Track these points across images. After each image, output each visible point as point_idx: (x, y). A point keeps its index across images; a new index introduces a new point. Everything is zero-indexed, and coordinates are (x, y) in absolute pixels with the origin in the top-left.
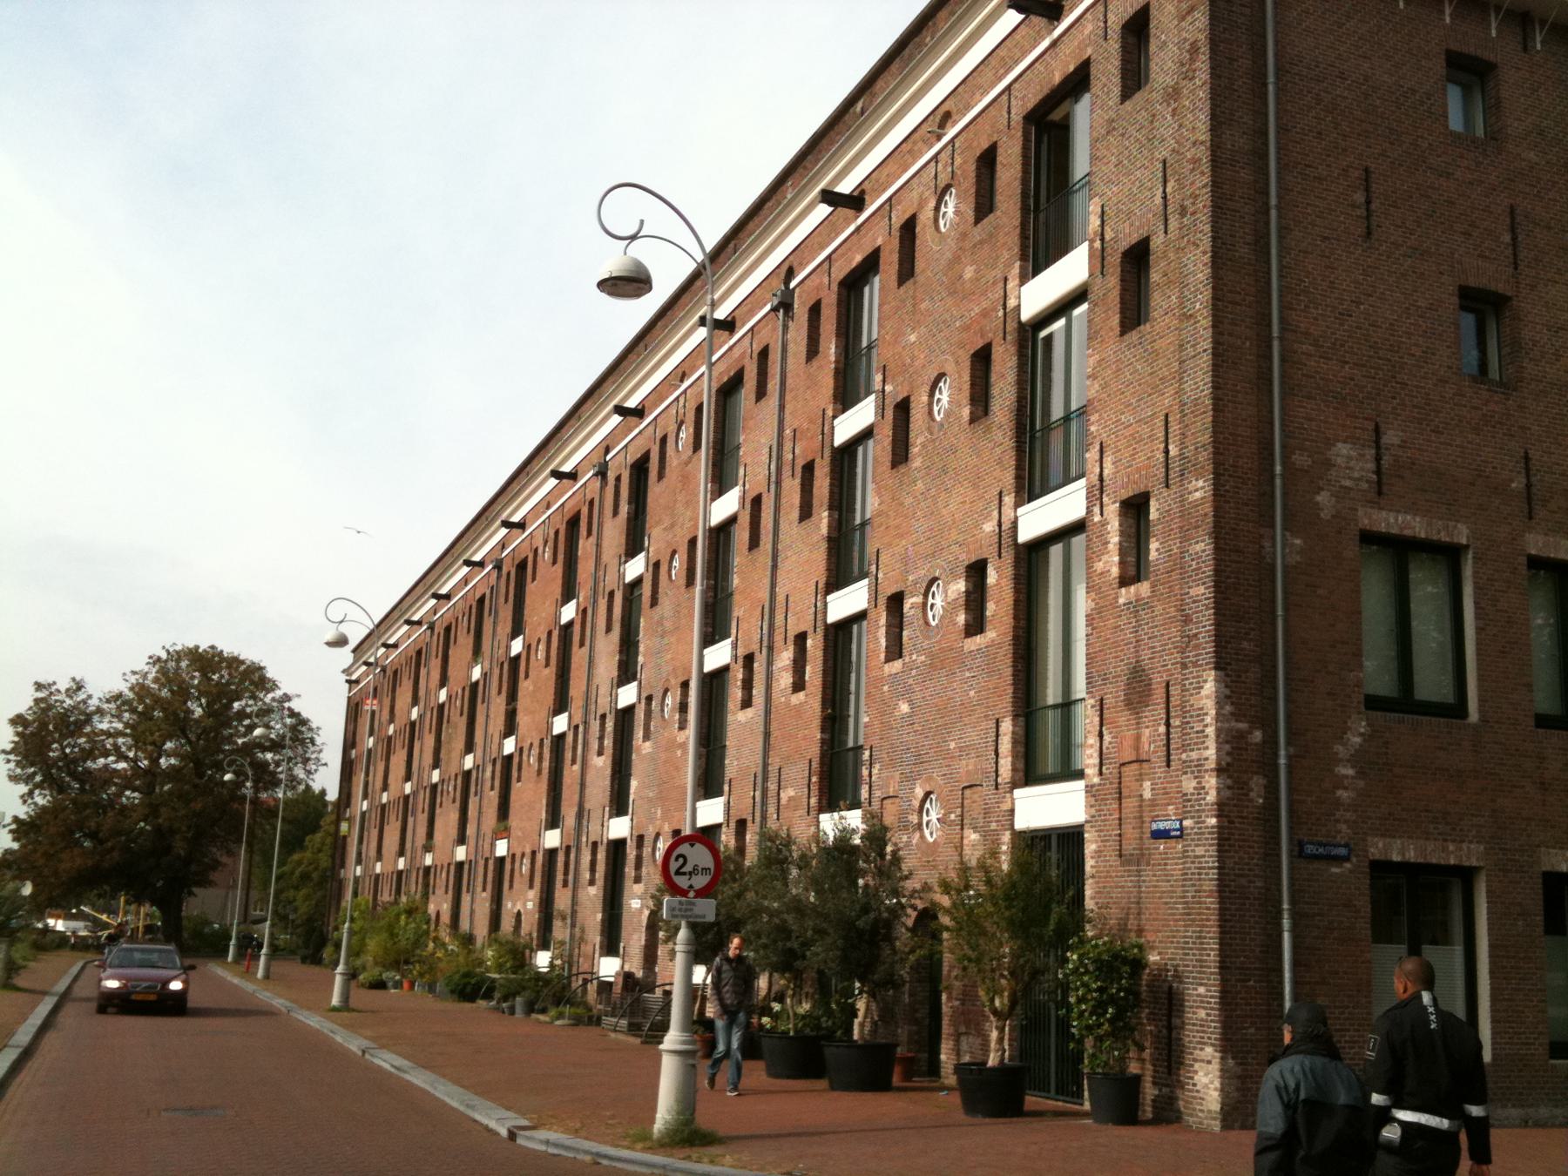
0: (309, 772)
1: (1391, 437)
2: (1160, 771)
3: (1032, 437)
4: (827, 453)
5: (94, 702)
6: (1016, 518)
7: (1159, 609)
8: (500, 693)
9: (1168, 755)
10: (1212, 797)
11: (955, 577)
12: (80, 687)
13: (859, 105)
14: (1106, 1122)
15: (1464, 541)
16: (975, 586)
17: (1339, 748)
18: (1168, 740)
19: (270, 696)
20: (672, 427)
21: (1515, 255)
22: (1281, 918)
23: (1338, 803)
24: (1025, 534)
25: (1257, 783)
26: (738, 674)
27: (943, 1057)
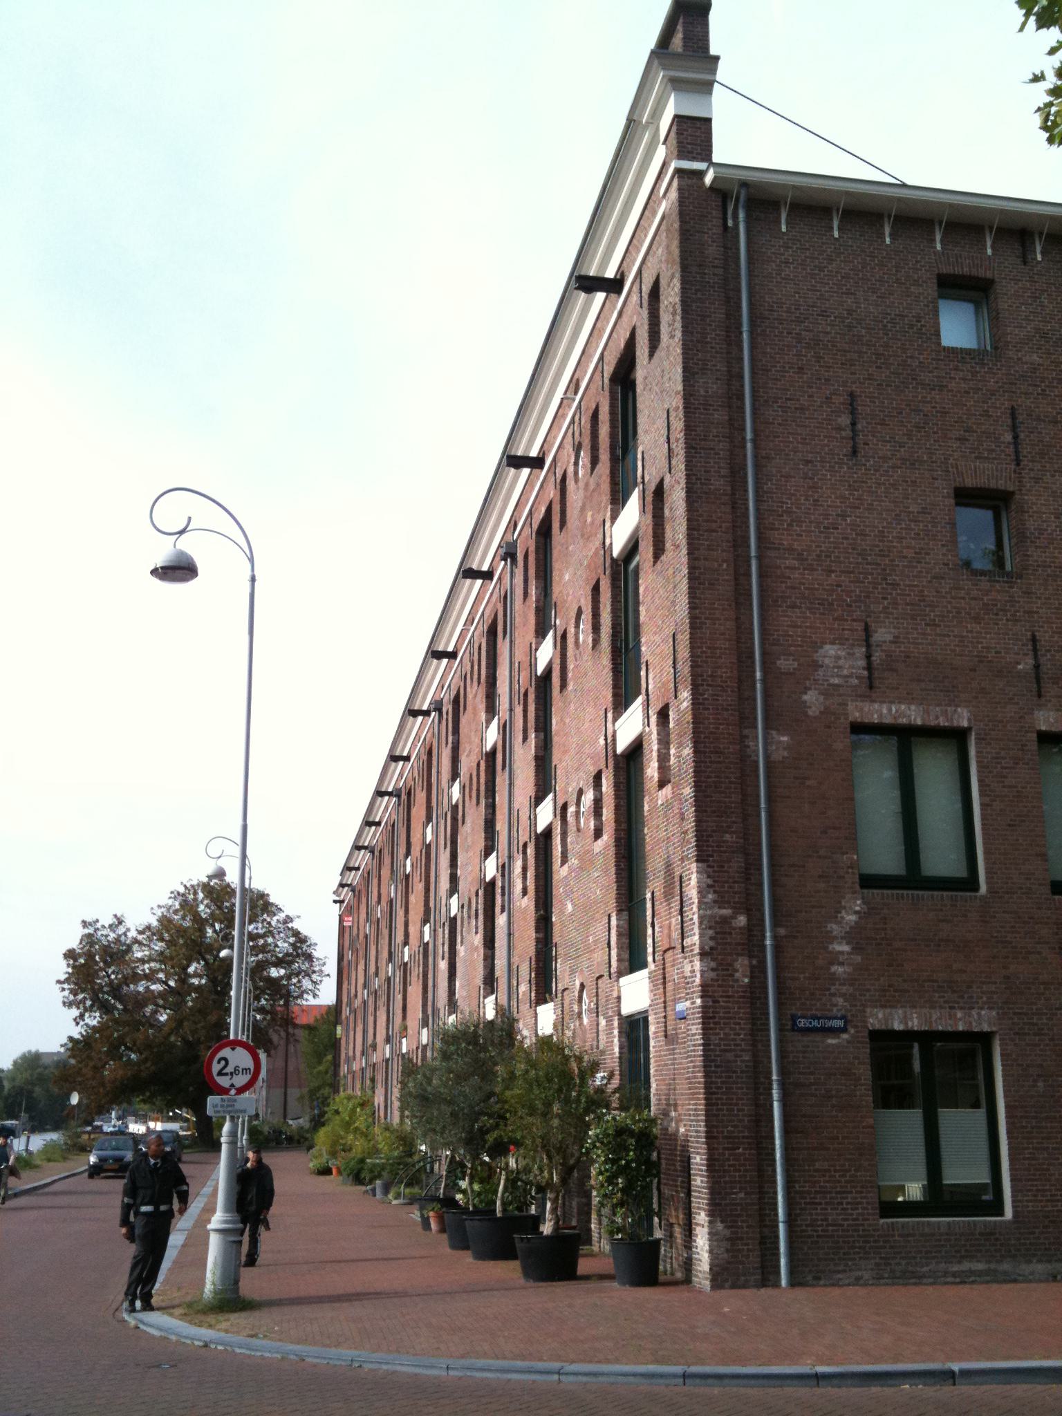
0: (315, 983)
1: (882, 635)
5: (132, 934)
12: (120, 922)
14: (624, 1284)
15: (965, 724)
17: (834, 928)
19: (275, 918)
21: (1017, 452)
22: (771, 1089)
23: (833, 978)
25: (742, 966)
27: (593, 1226)
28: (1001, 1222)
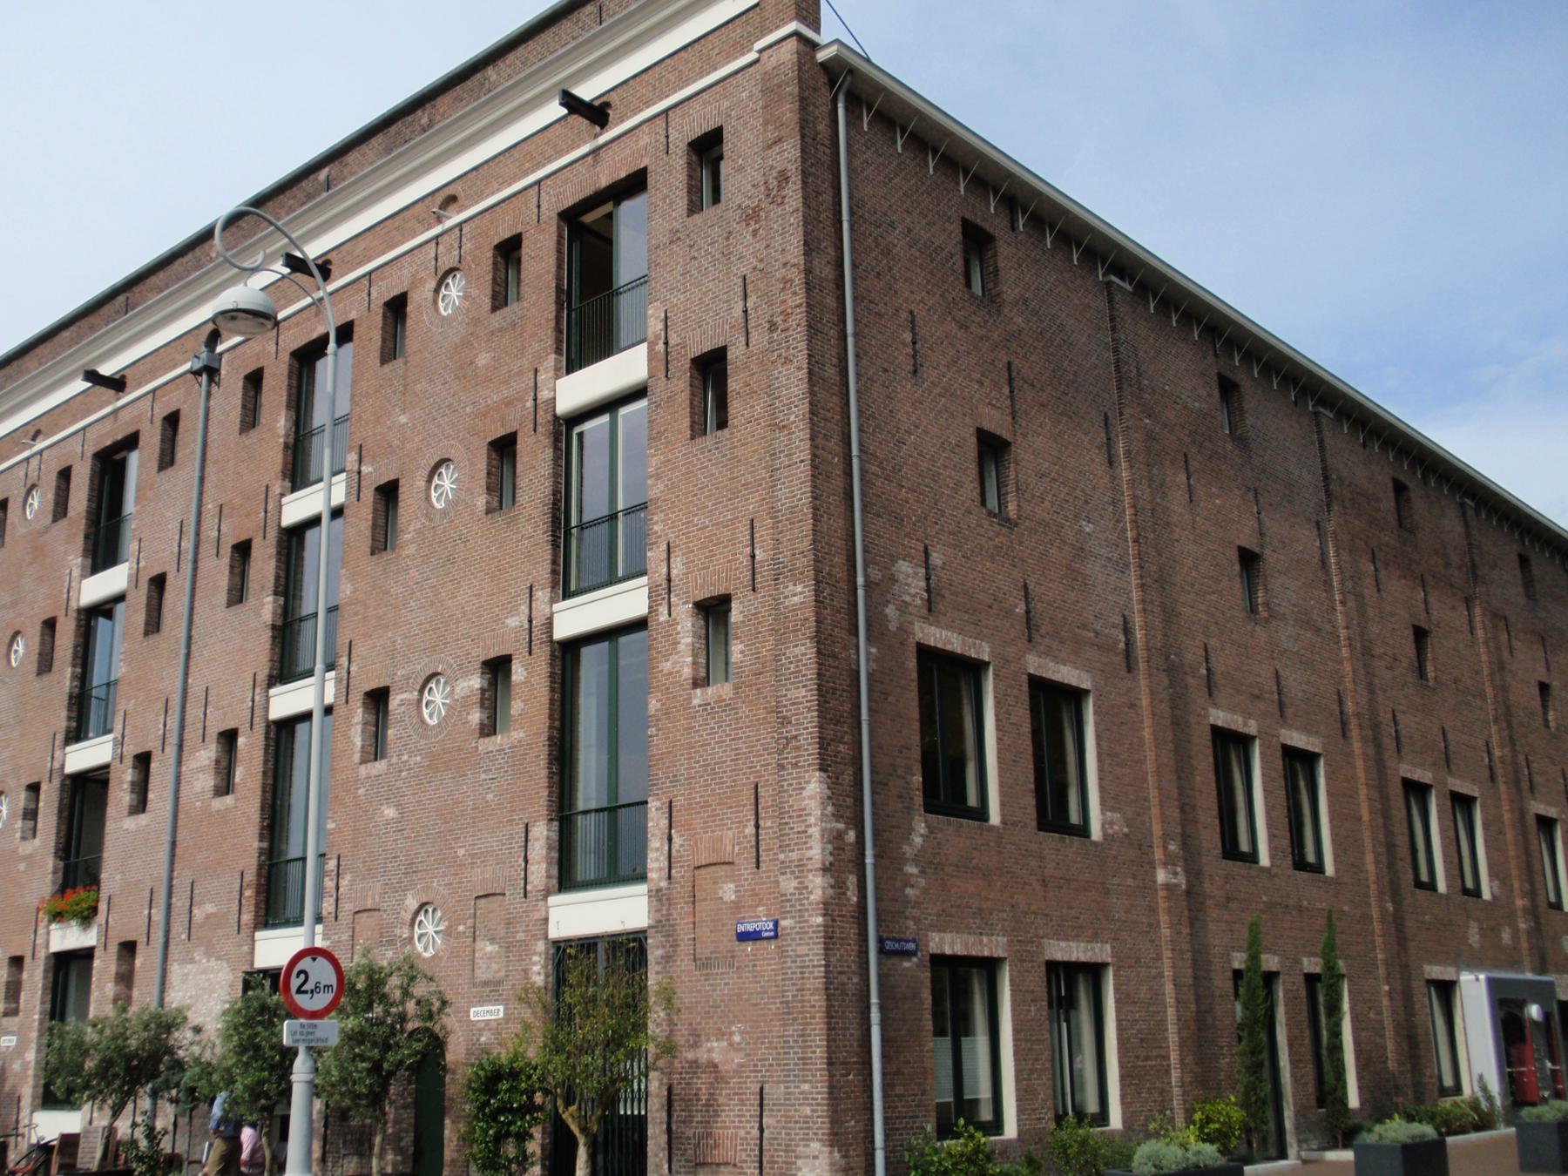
1: (936, 559)
3: (568, 533)
4: (272, 534)
6: (552, 614)
7: (744, 710)
9: (758, 856)
10: (817, 895)
11: (467, 674)
13: (323, 175)
16: (490, 684)
25: (852, 880)
28: (1103, 1133)
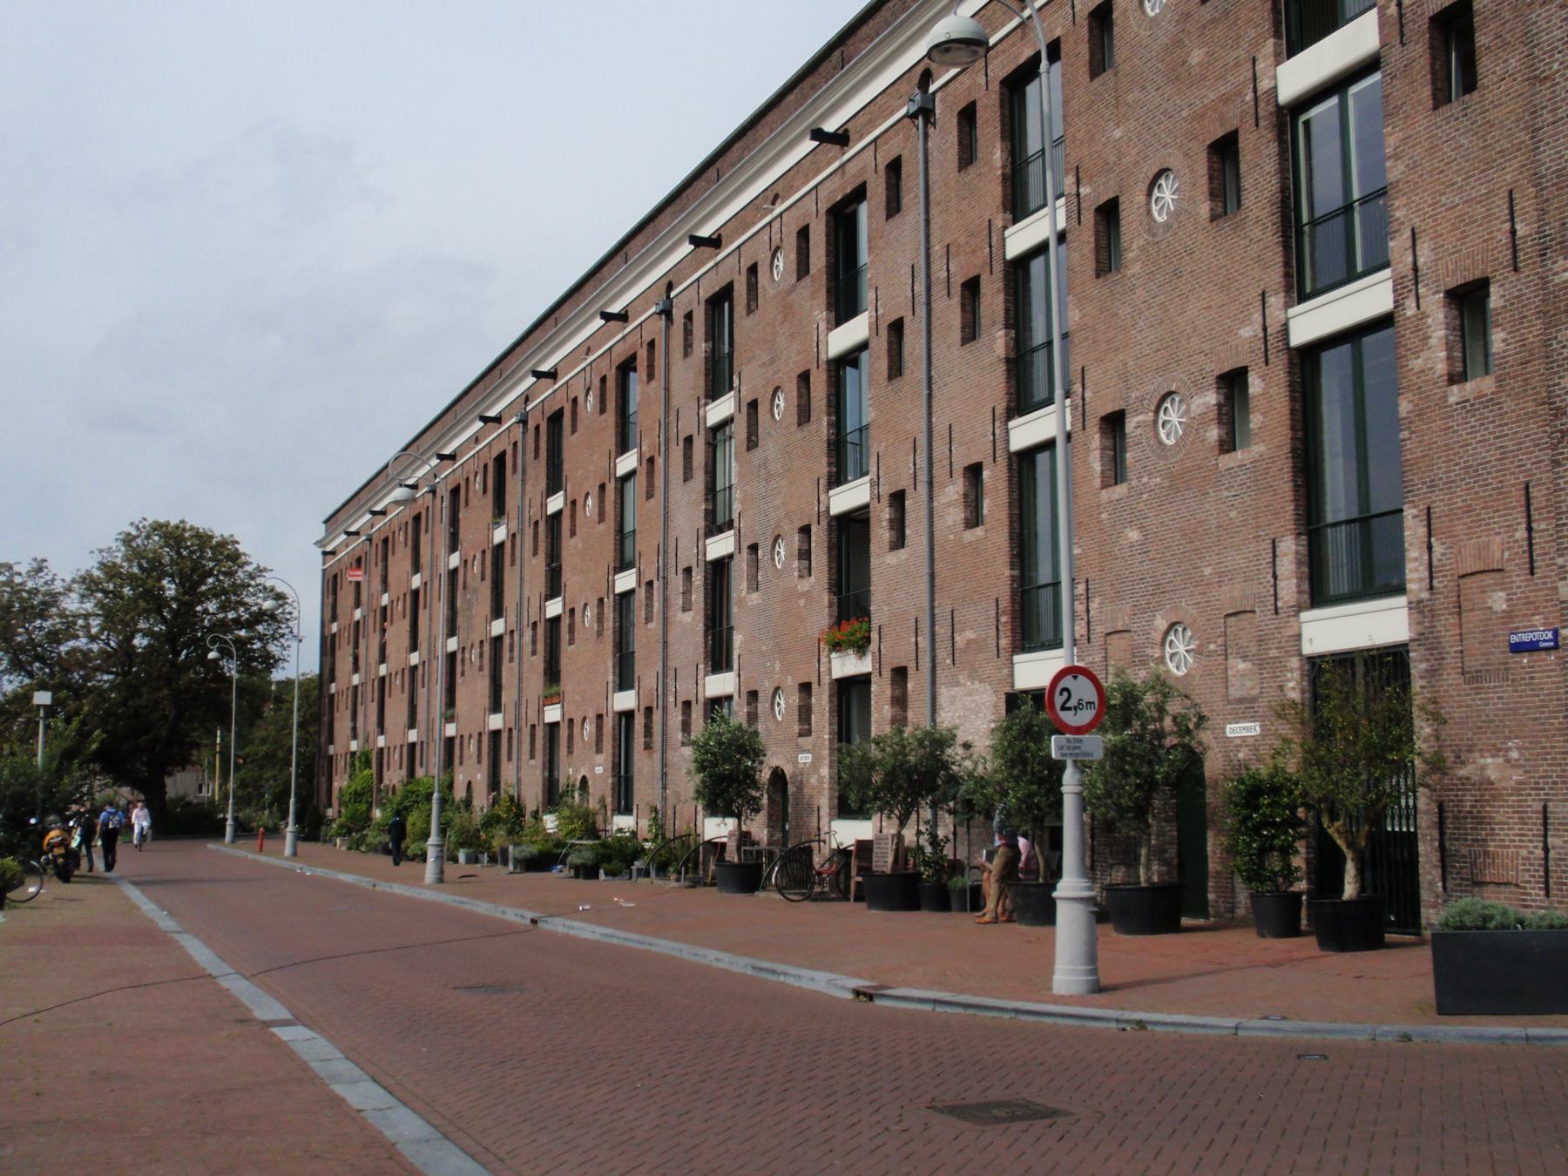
2: (1518, 578)
3: (1300, 233)
7: (1509, 405)
8: (535, 553)
9: (1532, 561)
11: (1201, 390)
18: (1530, 545)
20: (763, 258)
24: (1299, 337)
26: (641, 594)
